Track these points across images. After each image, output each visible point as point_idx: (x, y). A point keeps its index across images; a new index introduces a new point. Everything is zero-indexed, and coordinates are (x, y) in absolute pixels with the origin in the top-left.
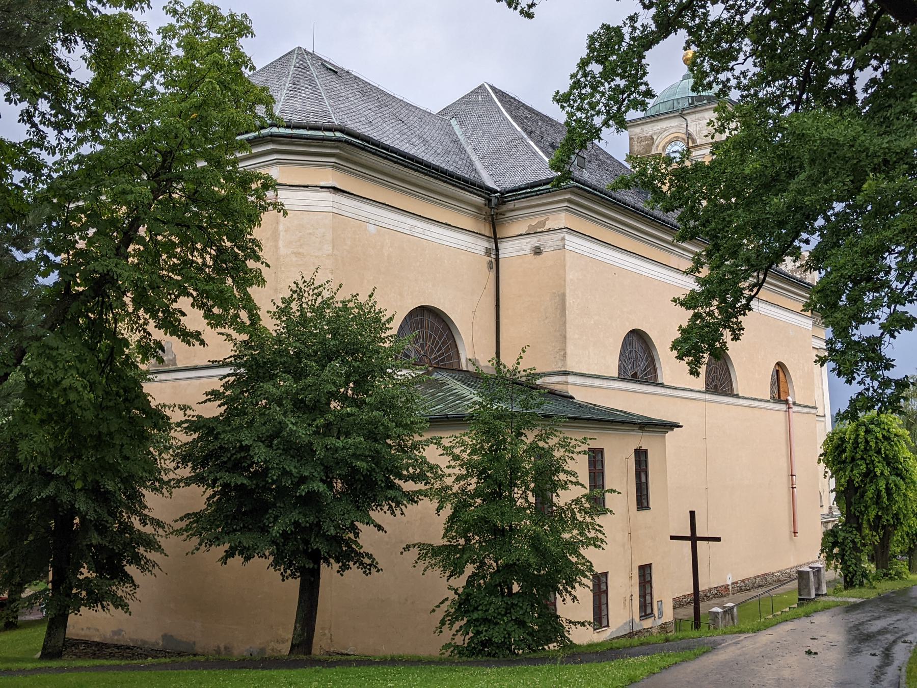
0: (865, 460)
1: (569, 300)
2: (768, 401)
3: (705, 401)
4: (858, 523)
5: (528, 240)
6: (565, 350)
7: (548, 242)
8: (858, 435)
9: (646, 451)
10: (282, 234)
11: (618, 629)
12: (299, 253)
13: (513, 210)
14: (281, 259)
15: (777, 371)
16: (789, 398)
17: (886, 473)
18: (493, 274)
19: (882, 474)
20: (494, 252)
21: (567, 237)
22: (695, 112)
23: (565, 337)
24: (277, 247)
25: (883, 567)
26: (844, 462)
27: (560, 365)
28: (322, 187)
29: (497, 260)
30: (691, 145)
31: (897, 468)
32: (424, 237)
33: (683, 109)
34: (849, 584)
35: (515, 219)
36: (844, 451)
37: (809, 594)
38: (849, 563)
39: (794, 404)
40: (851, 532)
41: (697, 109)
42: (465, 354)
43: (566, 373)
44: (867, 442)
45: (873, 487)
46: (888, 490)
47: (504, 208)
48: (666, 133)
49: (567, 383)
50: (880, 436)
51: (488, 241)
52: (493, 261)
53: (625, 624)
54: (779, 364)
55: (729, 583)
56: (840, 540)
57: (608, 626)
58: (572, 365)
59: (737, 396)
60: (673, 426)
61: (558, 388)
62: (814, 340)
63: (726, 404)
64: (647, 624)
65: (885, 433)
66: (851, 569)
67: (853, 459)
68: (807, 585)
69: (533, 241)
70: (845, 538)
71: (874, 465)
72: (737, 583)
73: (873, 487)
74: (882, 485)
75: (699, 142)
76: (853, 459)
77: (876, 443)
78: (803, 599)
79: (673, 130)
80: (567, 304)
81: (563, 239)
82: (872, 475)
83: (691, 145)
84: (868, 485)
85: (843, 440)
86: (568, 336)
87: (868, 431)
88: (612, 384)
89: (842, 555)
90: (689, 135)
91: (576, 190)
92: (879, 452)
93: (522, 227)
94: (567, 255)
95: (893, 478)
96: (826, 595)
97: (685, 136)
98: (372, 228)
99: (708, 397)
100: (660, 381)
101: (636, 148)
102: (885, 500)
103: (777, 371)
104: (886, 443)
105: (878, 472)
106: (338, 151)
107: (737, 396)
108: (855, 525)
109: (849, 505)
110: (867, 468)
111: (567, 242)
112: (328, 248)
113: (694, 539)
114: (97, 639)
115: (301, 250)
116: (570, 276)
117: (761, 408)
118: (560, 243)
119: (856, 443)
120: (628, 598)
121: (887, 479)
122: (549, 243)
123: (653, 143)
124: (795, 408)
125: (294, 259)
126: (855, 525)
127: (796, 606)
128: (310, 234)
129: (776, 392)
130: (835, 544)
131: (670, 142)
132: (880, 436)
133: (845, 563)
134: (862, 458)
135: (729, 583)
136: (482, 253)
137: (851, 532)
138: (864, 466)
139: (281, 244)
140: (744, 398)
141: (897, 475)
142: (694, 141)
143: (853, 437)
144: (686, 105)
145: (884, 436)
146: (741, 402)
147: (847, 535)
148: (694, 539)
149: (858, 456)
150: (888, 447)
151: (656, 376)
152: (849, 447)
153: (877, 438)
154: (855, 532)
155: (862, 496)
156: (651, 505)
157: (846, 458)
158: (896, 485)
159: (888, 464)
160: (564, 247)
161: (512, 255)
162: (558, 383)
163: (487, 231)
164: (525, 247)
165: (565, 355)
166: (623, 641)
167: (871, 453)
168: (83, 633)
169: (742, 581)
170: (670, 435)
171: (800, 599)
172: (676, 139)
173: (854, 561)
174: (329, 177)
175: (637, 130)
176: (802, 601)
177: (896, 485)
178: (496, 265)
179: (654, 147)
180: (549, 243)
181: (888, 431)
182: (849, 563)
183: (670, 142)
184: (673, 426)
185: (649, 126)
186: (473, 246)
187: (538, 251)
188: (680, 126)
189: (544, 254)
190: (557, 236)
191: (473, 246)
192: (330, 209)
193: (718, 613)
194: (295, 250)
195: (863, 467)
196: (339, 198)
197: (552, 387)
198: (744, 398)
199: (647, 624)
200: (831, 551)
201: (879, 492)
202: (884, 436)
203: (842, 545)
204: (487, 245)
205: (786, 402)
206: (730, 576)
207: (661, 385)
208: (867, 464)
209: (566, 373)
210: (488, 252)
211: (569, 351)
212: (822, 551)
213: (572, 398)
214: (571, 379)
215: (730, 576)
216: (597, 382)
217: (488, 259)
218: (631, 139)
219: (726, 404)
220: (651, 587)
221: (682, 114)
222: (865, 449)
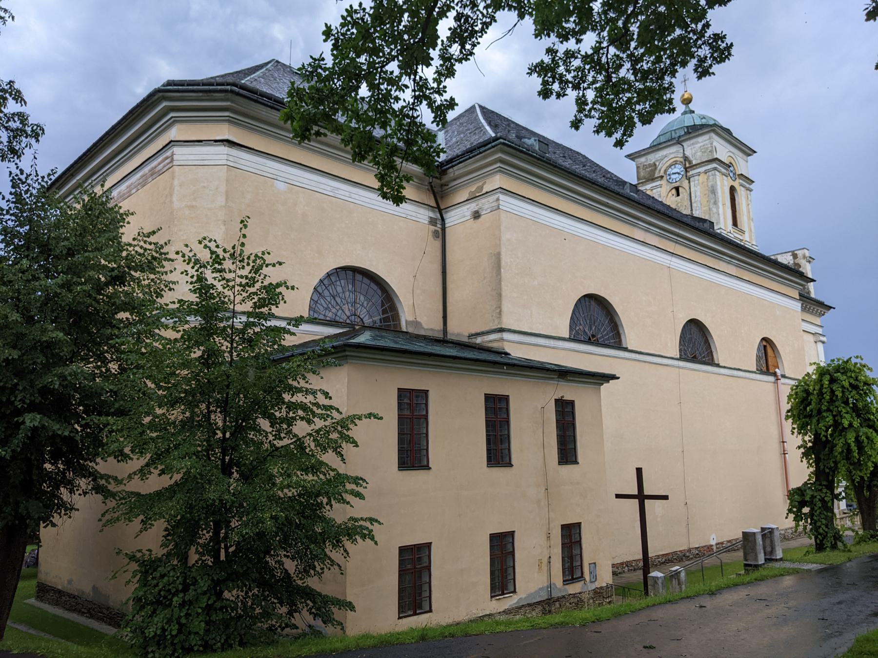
0: (832, 411)
1: (505, 260)
2: (755, 372)
3: (679, 367)
4: (828, 480)
5: (468, 206)
6: (500, 307)
7: (485, 204)
8: (822, 386)
9: (572, 403)
10: (176, 189)
11: (529, 596)
12: (193, 207)
13: (455, 180)
14: (175, 213)
15: (765, 347)
16: (777, 370)
17: (856, 424)
18: (438, 244)
19: (851, 425)
20: (439, 222)
21: (502, 197)
22: (690, 139)
23: (500, 295)
24: (171, 202)
25: (870, 529)
26: (810, 416)
27: (496, 322)
28: (216, 141)
29: (444, 229)
30: (688, 165)
31: (869, 419)
32: (350, 200)
33: (680, 137)
34: (820, 547)
35: (457, 189)
36: (810, 404)
37: (756, 559)
38: (818, 524)
39: (784, 376)
40: (821, 490)
41: (691, 135)
42: (406, 316)
43: (501, 330)
44: (833, 392)
45: (842, 440)
46: (857, 440)
47: (446, 179)
48: (666, 159)
49: (502, 340)
50: (846, 384)
51: (433, 211)
52: (440, 230)
53: (540, 589)
54: (764, 339)
55: (713, 543)
56: (807, 498)
57: (514, 592)
58: (508, 322)
59: (718, 366)
60: (614, 377)
61: (495, 345)
62: (804, 324)
63: (703, 371)
64: (574, 588)
65: (852, 381)
66: (821, 531)
67: (819, 412)
68: (754, 549)
69: (473, 206)
70: (813, 497)
71: (841, 416)
72: (722, 543)
73: (842, 440)
74: (851, 437)
75: (694, 162)
76: (819, 412)
77: (843, 392)
78: (750, 565)
79: (672, 156)
80: (503, 263)
81: (498, 199)
82: (840, 428)
83: (688, 165)
84: (837, 439)
85: (807, 392)
86: (503, 294)
87: (833, 381)
88: (561, 344)
89: (811, 515)
90: (686, 158)
91: (506, 148)
92: (846, 403)
93: (463, 195)
94: (503, 216)
95: (865, 430)
96: (781, 559)
97: (682, 160)
98: (281, 186)
99: (682, 364)
100: (624, 346)
101: (642, 174)
102: (856, 454)
103: (765, 347)
104: (854, 392)
105: (846, 423)
106: (228, 103)
107: (718, 366)
108: (825, 483)
109: (817, 461)
110: (834, 420)
111: (501, 202)
112: (221, 200)
113: (641, 497)
114: (60, 587)
115: (194, 203)
116: (506, 236)
117: (745, 378)
118: (495, 204)
119: (821, 394)
120: (545, 560)
121: (857, 431)
122: (486, 207)
123: (656, 169)
124: (783, 380)
125: (187, 212)
126: (825, 483)
127: (743, 572)
128: (204, 187)
129: (764, 365)
130: (803, 504)
131: (670, 166)
132: (846, 384)
133: (815, 523)
134: (828, 410)
135: (713, 543)
136: (426, 222)
137: (821, 490)
138: (831, 417)
139: (175, 199)
140: (725, 367)
141: (870, 427)
142: (690, 162)
143: (817, 388)
144: (683, 133)
145: (851, 384)
146: (722, 371)
147: (816, 494)
148: (641, 497)
149: (824, 408)
150: (857, 397)
151: (620, 341)
152: (814, 398)
153: (843, 387)
154: (825, 491)
155: (831, 451)
156: (580, 459)
157: (811, 410)
158: (868, 438)
159: (858, 416)
160: (499, 208)
161: (456, 222)
162: (495, 340)
163: (433, 204)
164: (467, 214)
165: (500, 313)
166: (503, 618)
167: (837, 404)
168: (53, 580)
169: (729, 541)
170: (606, 388)
171: (746, 565)
172: (675, 163)
173: (824, 521)
174: (225, 131)
175: (643, 160)
176: (750, 567)
177: (868, 438)
178: (441, 234)
179: (657, 171)
180: (486, 207)
181: (856, 379)
182: (818, 524)
183: (670, 166)
184: (614, 377)
185: (652, 155)
186: (414, 214)
187: (476, 215)
188: (677, 152)
189: (482, 217)
190: (492, 198)
191: (414, 214)
192: (225, 162)
193: (657, 578)
194: (189, 203)
195: (830, 420)
196: (234, 152)
197: (490, 345)
198: (725, 367)
199: (574, 588)
200: (799, 510)
201: (849, 445)
202: (851, 384)
203: (811, 503)
204: (432, 215)
205: (775, 374)
206: (713, 536)
207: (626, 349)
208: (834, 416)
209: (501, 330)
210: (433, 222)
211: (505, 308)
212: (790, 511)
213: (507, 354)
214: (506, 336)
215: (713, 536)
216: (552, 343)
217: (433, 228)
218: (638, 168)
219: (703, 371)
220: (581, 549)
221: (679, 141)
222: (831, 399)
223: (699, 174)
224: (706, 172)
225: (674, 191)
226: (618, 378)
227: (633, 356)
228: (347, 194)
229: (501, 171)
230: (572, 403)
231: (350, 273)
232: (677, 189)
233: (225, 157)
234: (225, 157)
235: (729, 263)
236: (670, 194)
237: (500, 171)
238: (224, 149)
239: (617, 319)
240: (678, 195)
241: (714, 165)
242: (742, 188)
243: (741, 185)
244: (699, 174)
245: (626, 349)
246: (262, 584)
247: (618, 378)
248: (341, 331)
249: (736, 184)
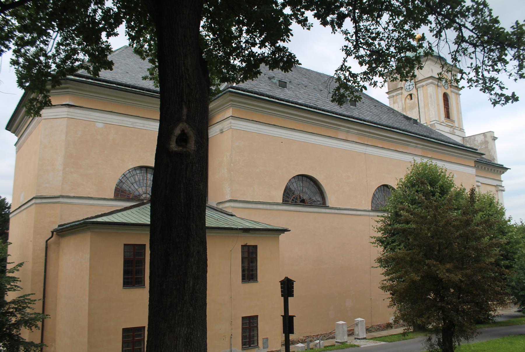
3: (369, 216)
28: (62, 105)
100: (327, 205)
170: (282, 237)
196: (72, 110)
207: (328, 207)
223: (423, 86)
224: (427, 85)
225: (409, 97)
226: (290, 231)
227: (333, 211)
228: (142, 125)
229: (232, 106)
230: (255, 247)
231: (145, 169)
232: (411, 95)
233: (66, 113)
234: (66, 113)
235: (416, 147)
236: (407, 99)
237: (231, 106)
238: (66, 109)
239: (322, 189)
240: (411, 99)
241: (430, 81)
242: (453, 94)
243: (452, 92)
244: (423, 86)
245: (328, 207)
246: (477, 248)
247: (290, 231)
248: (135, 204)
249: (448, 92)
